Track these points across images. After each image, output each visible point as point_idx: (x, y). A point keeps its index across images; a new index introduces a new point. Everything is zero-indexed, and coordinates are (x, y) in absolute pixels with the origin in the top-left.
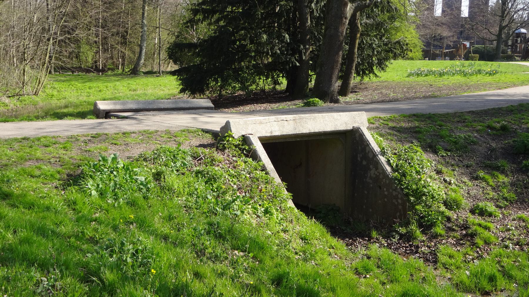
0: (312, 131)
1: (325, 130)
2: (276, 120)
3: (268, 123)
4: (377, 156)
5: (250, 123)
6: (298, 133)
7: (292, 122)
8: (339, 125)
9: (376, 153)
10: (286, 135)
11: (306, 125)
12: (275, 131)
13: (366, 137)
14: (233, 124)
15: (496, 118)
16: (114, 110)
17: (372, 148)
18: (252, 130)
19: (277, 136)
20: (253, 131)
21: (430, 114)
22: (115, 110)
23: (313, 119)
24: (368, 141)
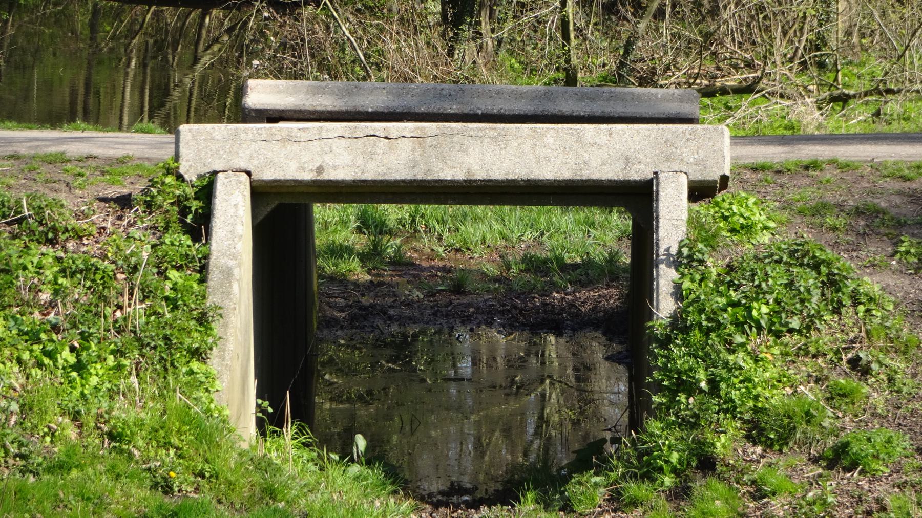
0: (480, 175)
1: (532, 177)
2: (347, 135)
3: (316, 143)
4: (657, 266)
5: (250, 137)
6: (419, 177)
7: (406, 146)
8: (593, 164)
9: (658, 255)
10: (374, 181)
11: (460, 155)
12: (335, 168)
13: (657, 207)
14: (189, 137)
15: (557, 293)
16: (295, 111)
17: (658, 240)
18: (251, 157)
19: (337, 182)
20: (256, 162)
21: (895, 163)
22: (300, 111)
23: (495, 139)
24: (657, 217)
